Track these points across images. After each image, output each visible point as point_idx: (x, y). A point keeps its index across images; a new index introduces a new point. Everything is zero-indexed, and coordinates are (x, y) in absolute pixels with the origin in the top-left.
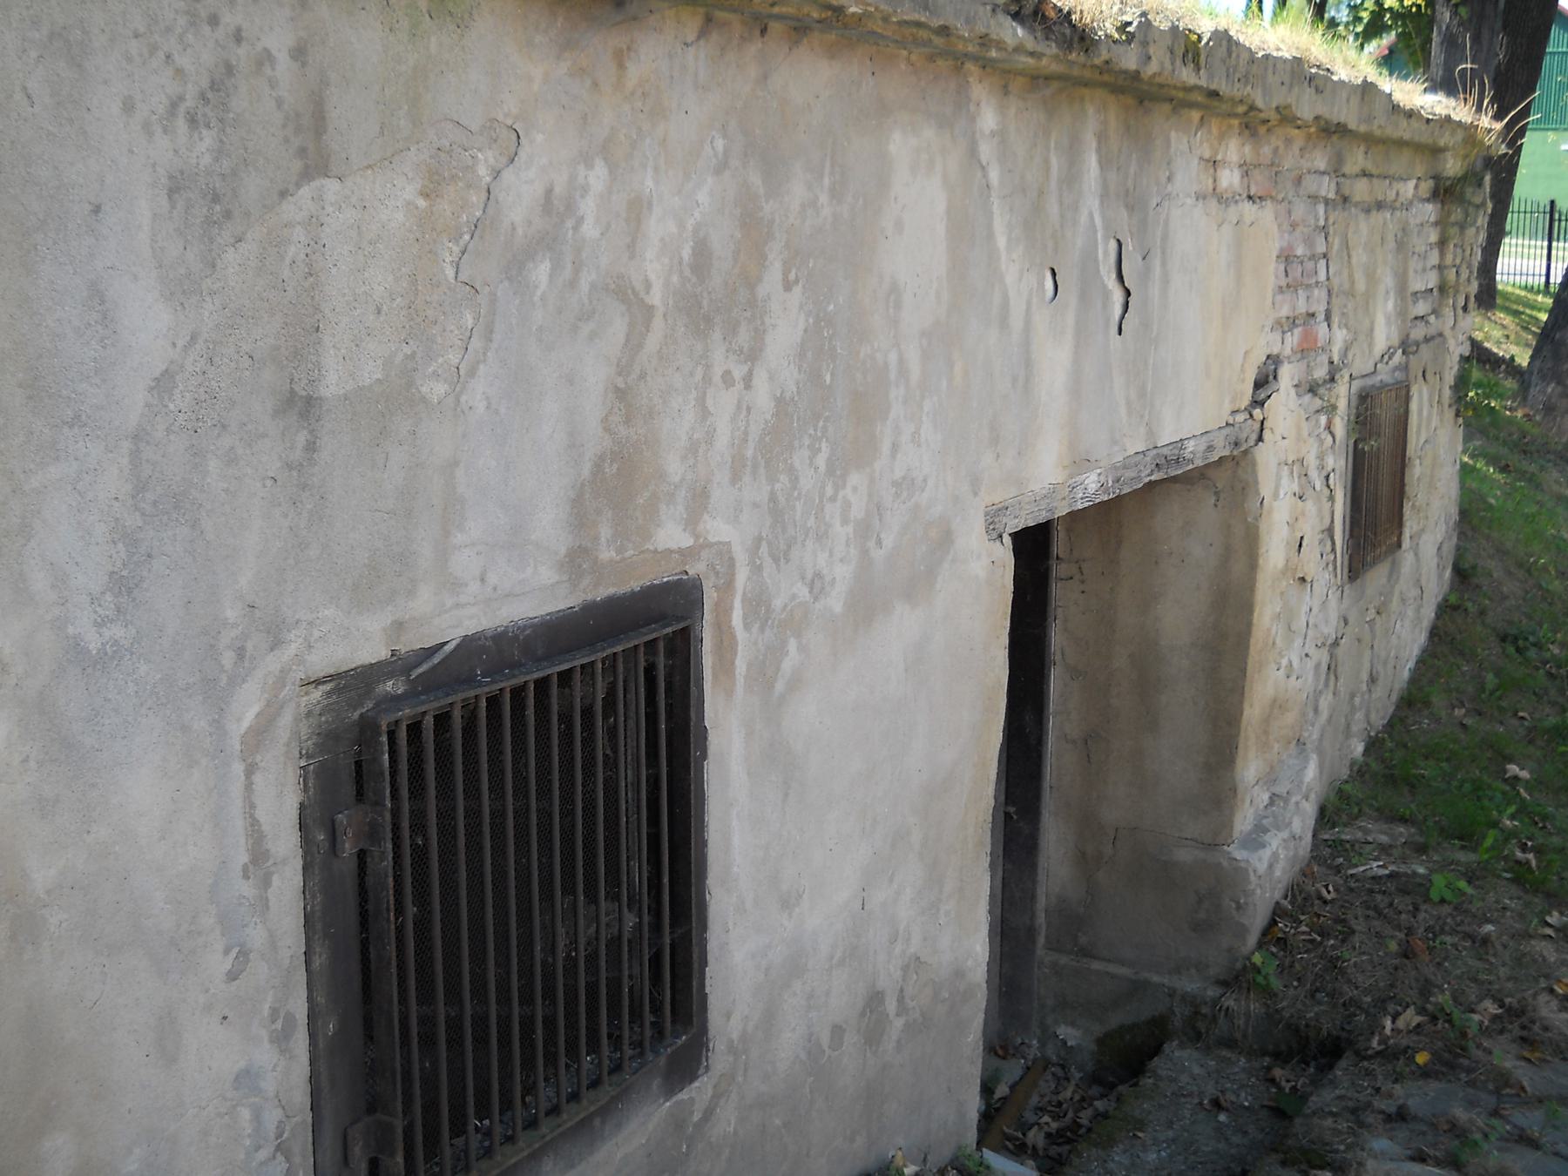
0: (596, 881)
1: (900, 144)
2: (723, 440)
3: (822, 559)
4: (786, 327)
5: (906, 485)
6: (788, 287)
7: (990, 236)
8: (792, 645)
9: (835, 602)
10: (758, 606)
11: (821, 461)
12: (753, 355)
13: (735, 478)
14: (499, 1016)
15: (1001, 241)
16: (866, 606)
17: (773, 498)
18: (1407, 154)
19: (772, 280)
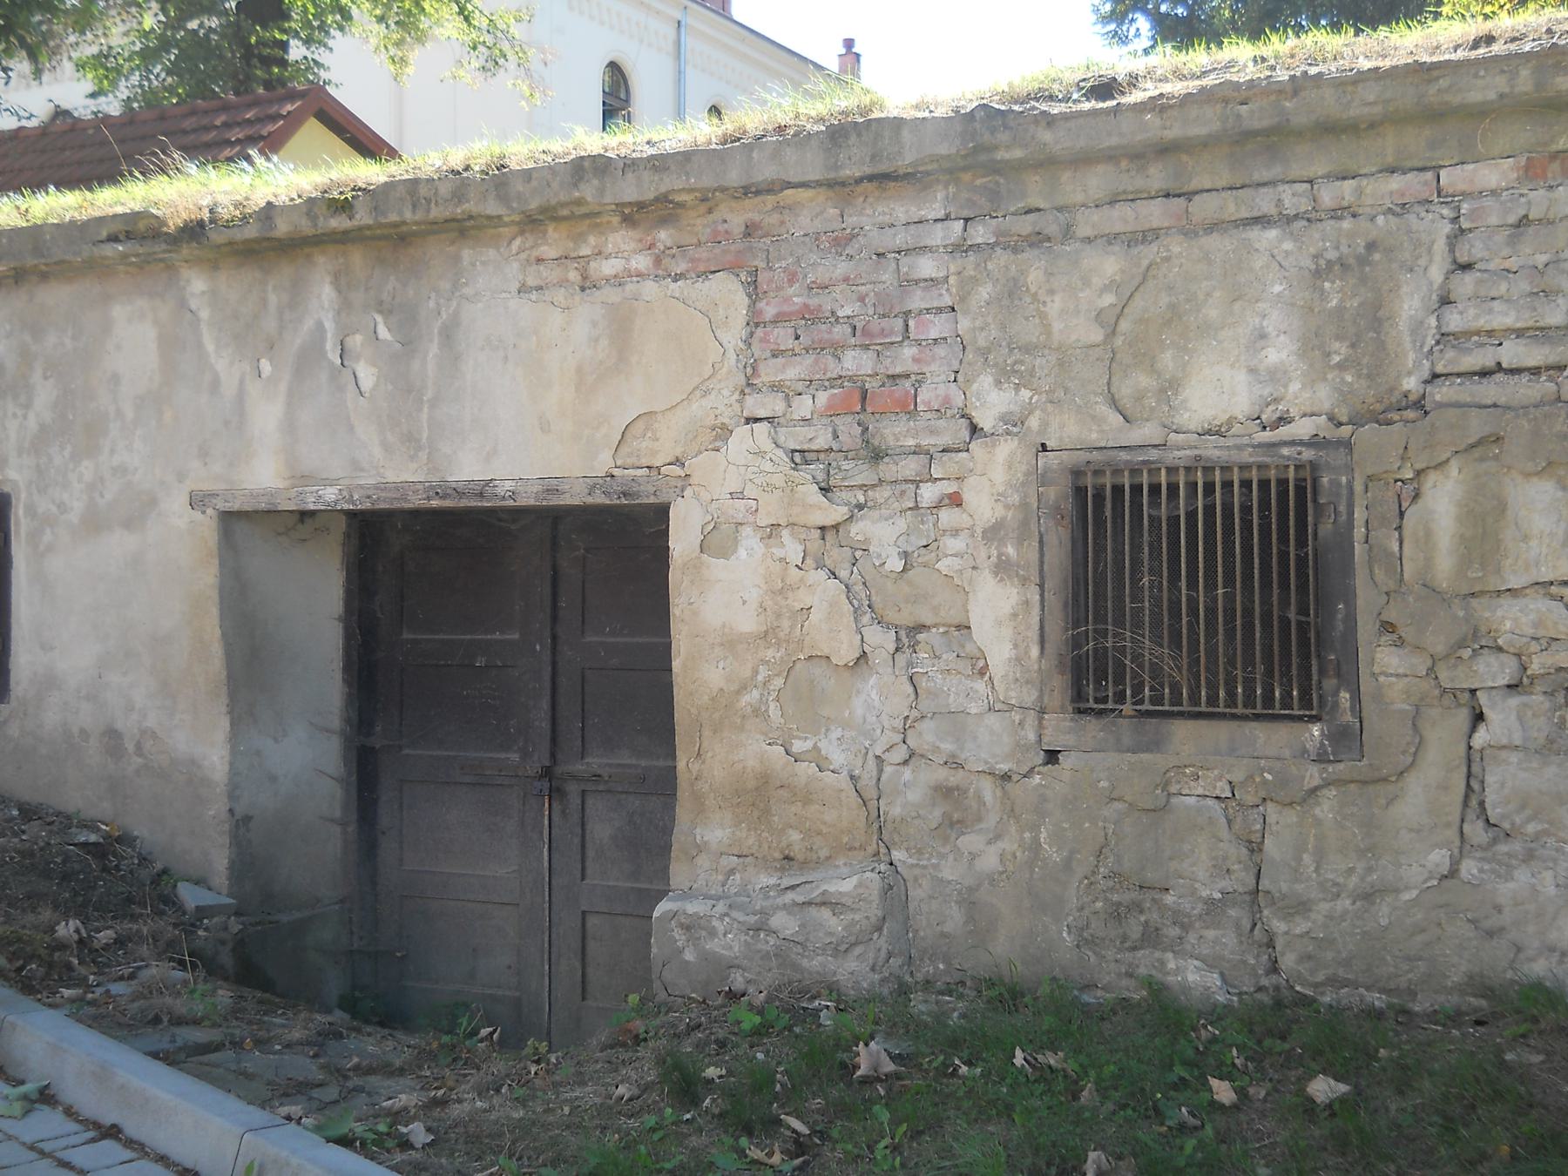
0: (1243, 557)
1: (119, 311)
2: (426, 410)
3: (65, 496)
4: (45, 394)
5: (121, 470)
6: (46, 378)
7: (200, 345)
8: (48, 531)
9: (74, 517)
10: (31, 510)
11: (67, 453)
12: (27, 406)
13: (20, 455)
14: (1169, 600)
15: (210, 347)
16: (94, 523)
17: (38, 465)
18: (865, 184)
19: (37, 376)
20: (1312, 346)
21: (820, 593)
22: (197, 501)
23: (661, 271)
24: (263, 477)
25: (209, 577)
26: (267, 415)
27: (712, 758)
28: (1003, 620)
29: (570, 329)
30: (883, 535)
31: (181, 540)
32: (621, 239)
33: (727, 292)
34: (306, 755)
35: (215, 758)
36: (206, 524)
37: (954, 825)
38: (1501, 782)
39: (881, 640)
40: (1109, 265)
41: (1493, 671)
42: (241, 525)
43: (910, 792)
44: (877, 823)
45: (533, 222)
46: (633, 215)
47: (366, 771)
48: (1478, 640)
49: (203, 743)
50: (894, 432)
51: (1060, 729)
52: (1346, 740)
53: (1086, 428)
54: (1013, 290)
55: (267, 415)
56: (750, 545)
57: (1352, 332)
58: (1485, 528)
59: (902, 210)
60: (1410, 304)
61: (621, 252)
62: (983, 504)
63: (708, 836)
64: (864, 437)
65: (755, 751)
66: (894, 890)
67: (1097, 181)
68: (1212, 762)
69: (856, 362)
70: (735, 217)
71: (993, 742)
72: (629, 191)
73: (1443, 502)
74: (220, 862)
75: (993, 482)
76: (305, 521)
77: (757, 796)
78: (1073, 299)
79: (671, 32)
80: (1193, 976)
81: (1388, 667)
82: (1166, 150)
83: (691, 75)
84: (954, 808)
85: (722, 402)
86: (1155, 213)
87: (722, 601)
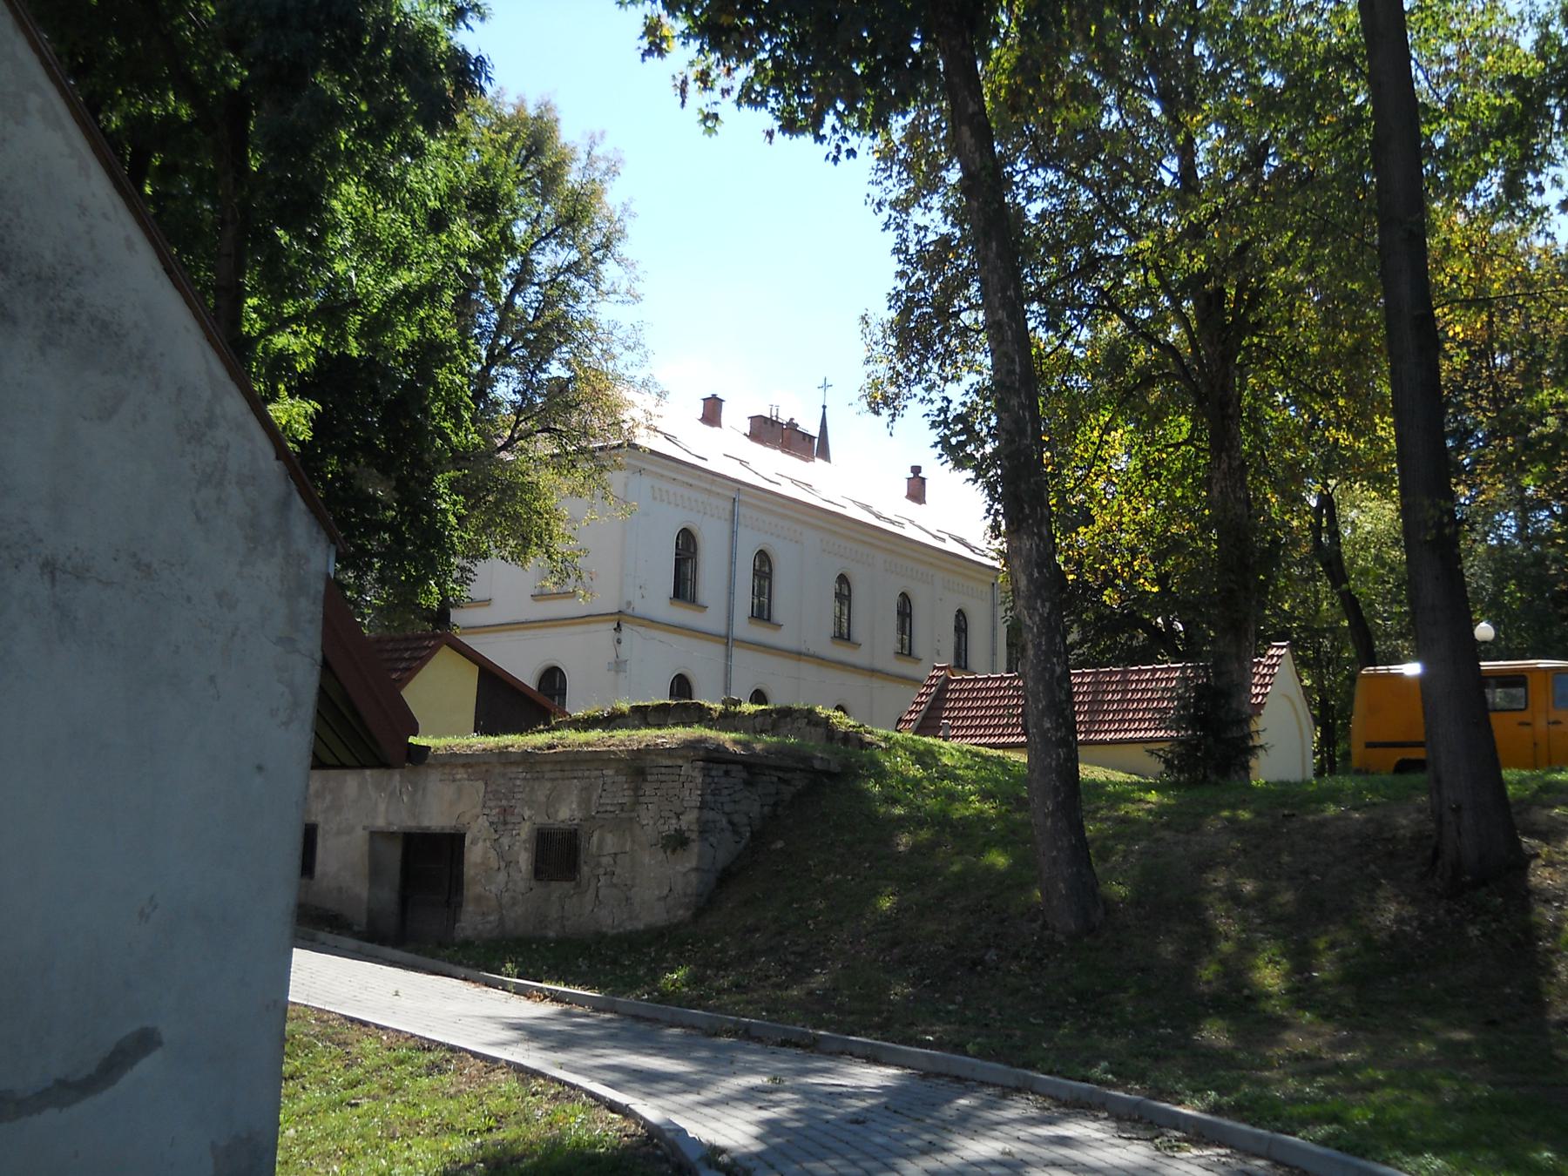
4: (329, 798)
20: (579, 805)
21: (492, 854)
22: (364, 828)
23: (469, 779)
24: (380, 823)
25: (366, 848)
26: (382, 807)
27: (471, 891)
28: (524, 859)
29: (449, 791)
30: (505, 841)
31: (360, 835)
32: (461, 770)
33: (480, 785)
34: (389, 895)
35: (365, 894)
36: (366, 833)
37: (514, 904)
38: (602, 892)
39: (503, 864)
40: (549, 785)
41: (601, 871)
42: (375, 835)
43: (506, 897)
44: (500, 905)
45: (443, 765)
46: (464, 766)
47: (404, 901)
48: (599, 865)
49: (361, 889)
50: (509, 819)
51: (533, 883)
52: (578, 885)
53: (541, 820)
54: (532, 789)
55: (382, 807)
56: (480, 844)
57: (585, 802)
58: (601, 841)
59: (514, 769)
60: (595, 797)
61: (461, 774)
62: (523, 836)
63: (469, 908)
64: (504, 821)
65: (478, 889)
66: (501, 920)
67: (548, 767)
68: (558, 888)
69: (504, 803)
70: (484, 768)
71: (522, 886)
72: (461, 761)
73: (595, 838)
74: (364, 921)
75: (525, 830)
76: (390, 835)
77: (479, 899)
78: (542, 792)
79: (729, 506)
80: (551, 934)
81: (585, 869)
82: (557, 762)
83: (741, 531)
84: (514, 902)
85: (478, 810)
86: (558, 774)
87: (475, 854)
